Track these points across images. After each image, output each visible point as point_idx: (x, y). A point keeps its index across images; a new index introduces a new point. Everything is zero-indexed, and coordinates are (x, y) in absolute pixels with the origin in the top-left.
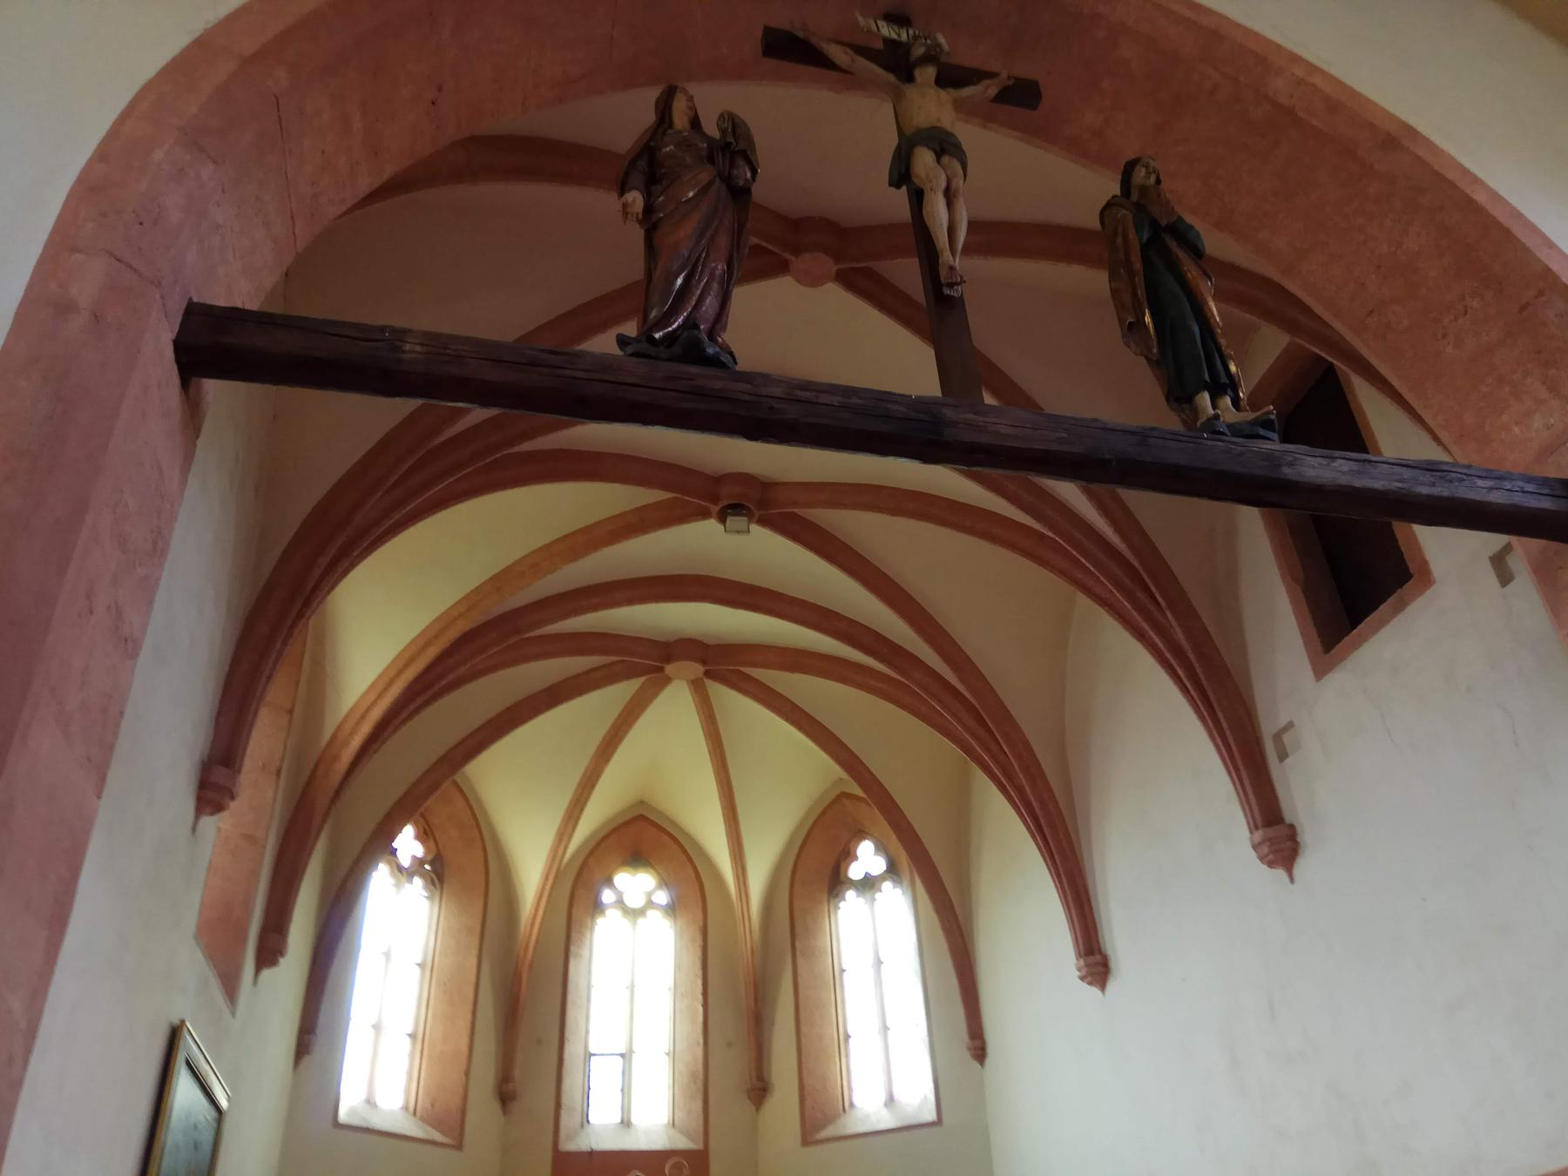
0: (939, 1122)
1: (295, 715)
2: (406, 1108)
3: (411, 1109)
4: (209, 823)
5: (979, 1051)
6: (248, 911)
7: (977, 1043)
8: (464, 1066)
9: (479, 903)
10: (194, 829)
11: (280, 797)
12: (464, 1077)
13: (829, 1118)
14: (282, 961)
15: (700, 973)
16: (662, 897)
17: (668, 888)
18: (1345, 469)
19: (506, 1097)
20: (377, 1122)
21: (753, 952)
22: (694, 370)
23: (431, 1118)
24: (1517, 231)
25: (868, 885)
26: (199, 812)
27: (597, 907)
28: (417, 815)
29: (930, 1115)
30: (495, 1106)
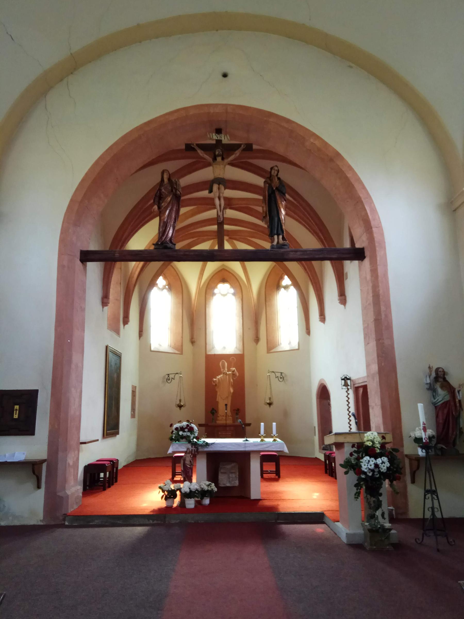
0: (298, 349)
1: (122, 269)
2: (169, 345)
3: (170, 346)
4: (106, 308)
5: (308, 332)
6: (119, 314)
7: (308, 331)
8: (181, 336)
9: (181, 295)
10: (103, 311)
11: (122, 288)
12: (181, 338)
13: (274, 347)
14: (129, 323)
15: (241, 311)
16: (232, 291)
17: (233, 288)
18: (299, 254)
19: (193, 342)
20: (161, 349)
21: (254, 306)
22: (166, 251)
23: (175, 348)
24: (357, 186)
25: (286, 287)
26: (103, 307)
27: (214, 294)
28: (162, 274)
29: (297, 348)
30: (190, 345)
